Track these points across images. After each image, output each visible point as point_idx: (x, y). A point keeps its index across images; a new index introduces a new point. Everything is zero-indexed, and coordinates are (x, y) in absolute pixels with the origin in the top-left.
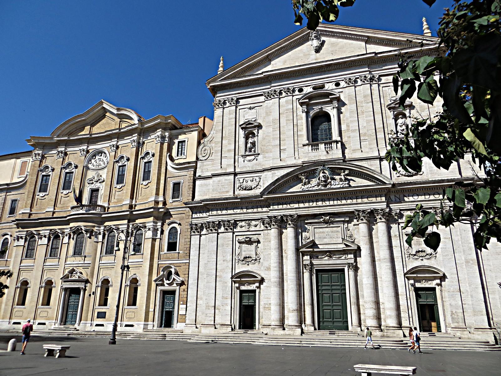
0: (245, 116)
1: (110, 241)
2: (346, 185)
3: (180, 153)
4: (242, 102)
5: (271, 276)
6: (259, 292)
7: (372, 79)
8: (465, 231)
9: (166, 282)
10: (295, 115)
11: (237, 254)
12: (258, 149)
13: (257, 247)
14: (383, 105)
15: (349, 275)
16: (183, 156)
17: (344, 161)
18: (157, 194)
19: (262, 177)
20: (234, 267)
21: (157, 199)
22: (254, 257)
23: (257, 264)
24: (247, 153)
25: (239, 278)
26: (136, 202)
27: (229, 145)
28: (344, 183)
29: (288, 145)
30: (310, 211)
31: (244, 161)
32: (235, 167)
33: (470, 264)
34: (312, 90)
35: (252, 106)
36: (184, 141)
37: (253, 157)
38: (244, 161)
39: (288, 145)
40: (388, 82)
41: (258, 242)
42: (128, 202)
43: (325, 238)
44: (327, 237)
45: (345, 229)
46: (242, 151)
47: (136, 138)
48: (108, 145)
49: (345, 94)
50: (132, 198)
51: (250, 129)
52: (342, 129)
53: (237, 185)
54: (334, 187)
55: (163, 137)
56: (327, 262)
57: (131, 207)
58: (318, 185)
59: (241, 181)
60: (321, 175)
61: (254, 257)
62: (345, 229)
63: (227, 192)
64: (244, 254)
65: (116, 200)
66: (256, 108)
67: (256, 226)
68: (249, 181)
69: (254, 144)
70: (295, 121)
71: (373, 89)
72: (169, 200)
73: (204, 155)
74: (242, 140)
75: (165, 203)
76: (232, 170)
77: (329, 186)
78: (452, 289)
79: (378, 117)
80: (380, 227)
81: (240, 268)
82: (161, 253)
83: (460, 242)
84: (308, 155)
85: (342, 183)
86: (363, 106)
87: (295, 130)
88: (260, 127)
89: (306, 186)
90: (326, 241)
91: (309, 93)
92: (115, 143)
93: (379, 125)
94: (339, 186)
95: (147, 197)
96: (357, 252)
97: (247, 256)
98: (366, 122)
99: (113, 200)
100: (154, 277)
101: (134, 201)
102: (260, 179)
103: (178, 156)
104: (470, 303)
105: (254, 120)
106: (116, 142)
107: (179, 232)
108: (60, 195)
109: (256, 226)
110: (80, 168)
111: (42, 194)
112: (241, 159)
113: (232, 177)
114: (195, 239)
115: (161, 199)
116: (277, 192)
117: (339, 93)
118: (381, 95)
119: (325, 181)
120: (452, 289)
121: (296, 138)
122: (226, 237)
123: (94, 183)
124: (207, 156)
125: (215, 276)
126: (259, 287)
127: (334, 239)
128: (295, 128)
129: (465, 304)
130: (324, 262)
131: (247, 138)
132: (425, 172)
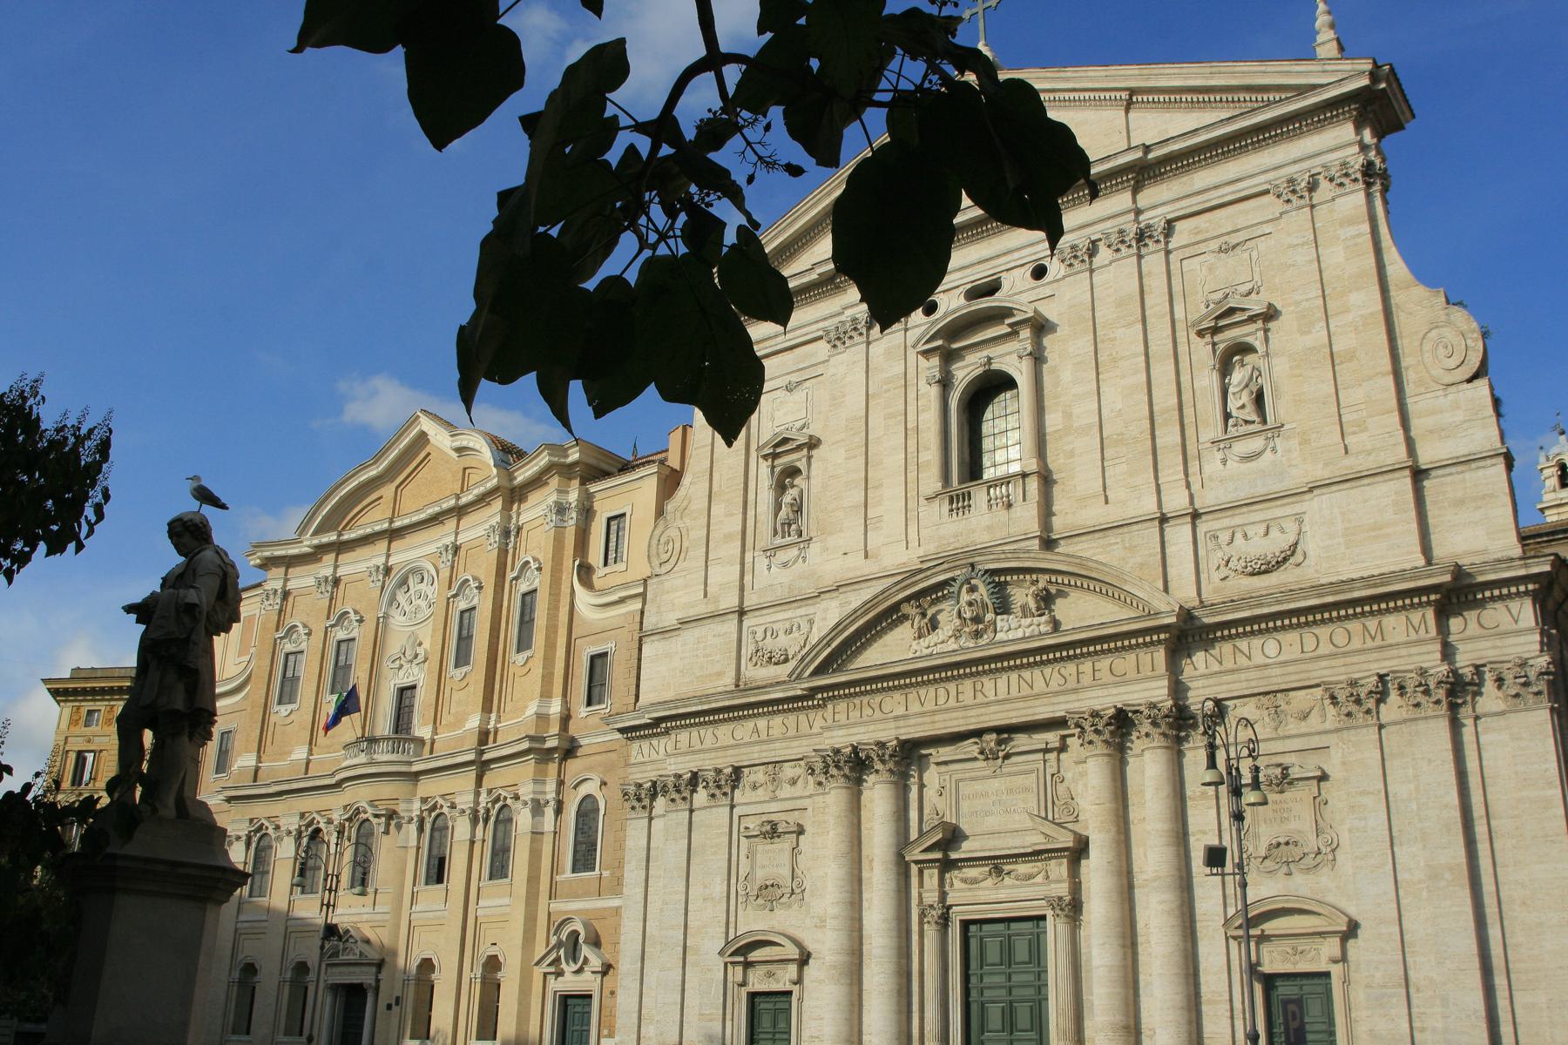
0: (1206, 278)
1: (500, 834)
2: (1043, 629)
3: (612, 555)
4: (1179, 226)
5: (827, 945)
6: (1346, 981)
7: (1141, 237)
8: (1430, 761)
9: (569, 968)
10: (912, 396)
11: (741, 878)
12: (810, 522)
13: (1319, 803)
14: (1180, 326)
15: (1055, 931)
16: (621, 566)
17: (1048, 544)
18: (546, 694)
19: (1306, 518)
20: (732, 919)
21: (543, 711)
22: (1312, 843)
23: (795, 907)
24: (779, 541)
25: (743, 952)
26: (498, 720)
27: (727, 522)
28: (1036, 620)
29: (889, 503)
30: (1356, 668)
31: (1224, 462)
32: (742, 589)
33: (1442, 884)
34: (962, 301)
35: (794, 378)
36: (623, 515)
37: (794, 552)
38: (1224, 462)
39: (889, 503)
40: (1199, 238)
41: (1323, 777)
42: (474, 722)
43: (988, 813)
44: (992, 805)
45: (1049, 778)
46: (765, 537)
47: (498, 518)
48: (432, 548)
49: (1062, 297)
50: (487, 707)
51: (1232, 334)
52: (1048, 430)
53: (747, 650)
54: (1011, 636)
55: (561, 510)
56: (993, 897)
57: (484, 736)
58: (957, 635)
59: (760, 636)
60: (965, 597)
61: (1312, 843)
62: (1049, 778)
63: (720, 674)
64: (761, 875)
65: (451, 719)
66: (808, 384)
67: (794, 782)
68: (781, 633)
69: (798, 508)
70: (911, 417)
71: (1150, 273)
72: (581, 711)
73: (665, 557)
74: (1208, 380)
75: (566, 719)
76: (1153, 507)
77: (985, 639)
78: (1378, 975)
79: (1163, 372)
80: (1148, 763)
81: (752, 922)
82: (558, 878)
83: (1414, 806)
84: (945, 532)
85: (1029, 620)
86: (1115, 339)
87: (912, 448)
88: (813, 444)
89: (924, 642)
90: (992, 822)
91: (954, 311)
92: (328, 572)
93: (1165, 397)
94: (1019, 634)
95: (525, 708)
96: (1079, 850)
97: (1282, 840)
98: (1122, 398)
99: (446, 719)
100: (540, 950)
101: (493, 716)
102: (1301, 522)
103: (606, 564)
104: (1439, 1025)
105: (798, 424)
106: (383, 559)
107: (602, 812)
108: (273, 718)
109: (794, 782)
110: (370, 625)
111: (284, 710)
112: (762, 562)
113: (731, 624)
114: (635, 831)
115: (555, 707)
116: (835, 669)
117: (1032, 306)
118: (1177, 287)
119: (977, 620)
120: (1378, 975)
121: (912, 476)
122: (712, 818)
123: (406, 666)
124: (674, 559)
125: (681, 949)
126: (799, 981)
127: (1016, 817)
128: (912, 443)
129: (1423, 1030)
130: (975, 895)
131: (781, 488)
132: (1310, 553)
